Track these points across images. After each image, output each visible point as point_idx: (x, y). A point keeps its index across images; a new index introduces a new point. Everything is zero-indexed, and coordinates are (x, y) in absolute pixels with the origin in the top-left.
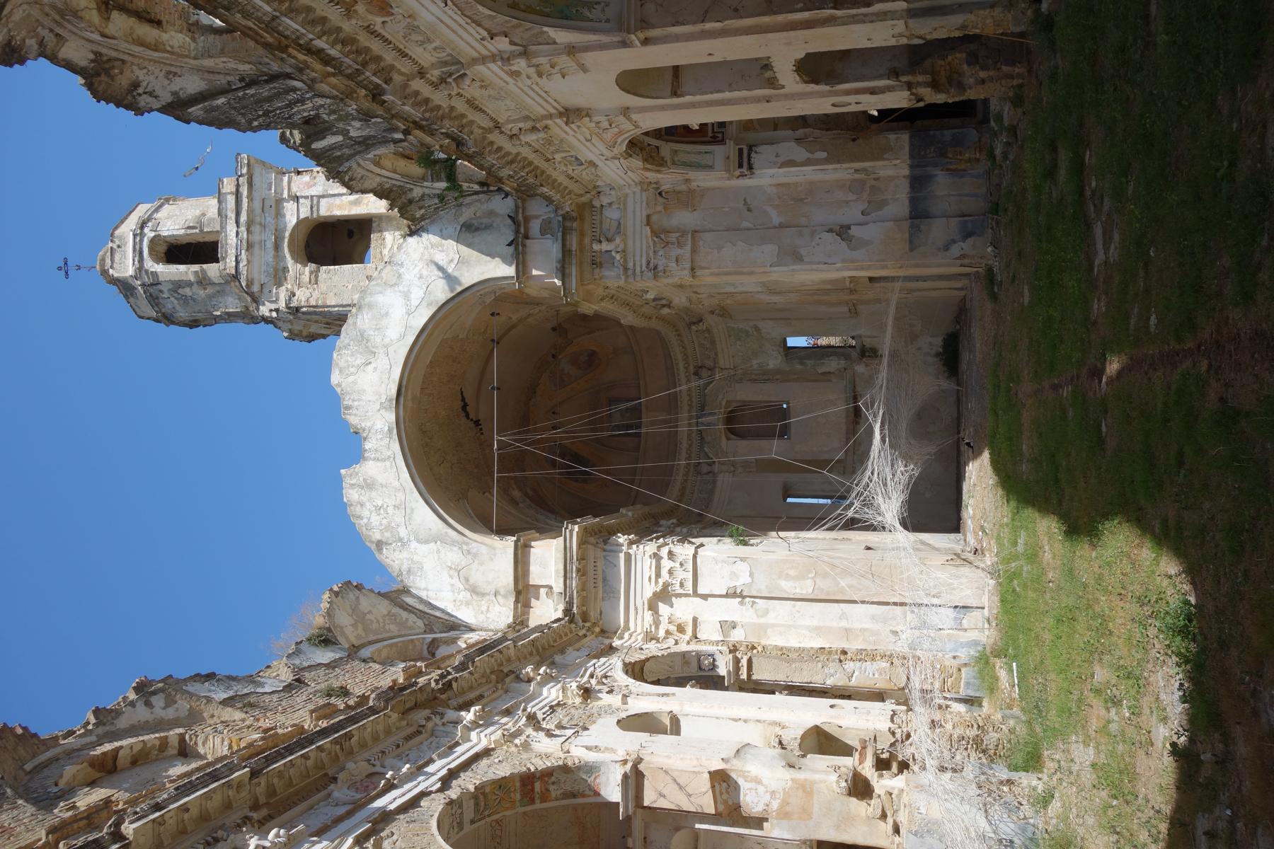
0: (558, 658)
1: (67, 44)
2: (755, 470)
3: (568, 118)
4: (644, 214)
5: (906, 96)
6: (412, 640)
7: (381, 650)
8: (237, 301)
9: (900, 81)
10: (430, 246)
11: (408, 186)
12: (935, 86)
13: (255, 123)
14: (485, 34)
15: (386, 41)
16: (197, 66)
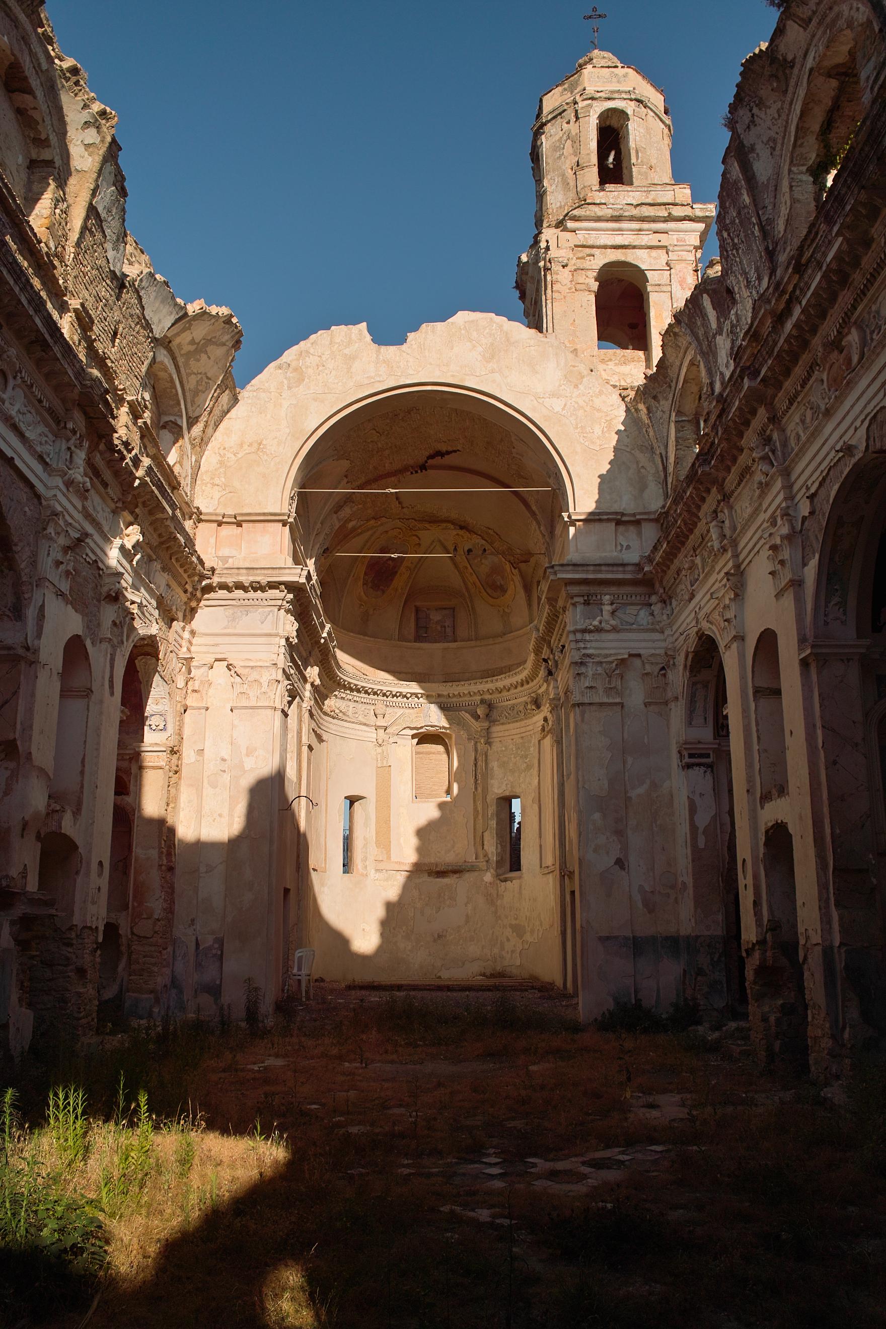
0: (157, 565)
1: (801, 30)
2: (379, 765)
3: (732, 575)
4: (642, 652)
5: (752, 939)
6: (179, 404)
7: (166, 371)
8: (558, 205)
9: (767, 932)
10: (608, 419)
11: (671, 395)
12: (761, 970)
13: (725, 235)
14: (813, 490)
15: (804, 384)
16: (782, 173)
